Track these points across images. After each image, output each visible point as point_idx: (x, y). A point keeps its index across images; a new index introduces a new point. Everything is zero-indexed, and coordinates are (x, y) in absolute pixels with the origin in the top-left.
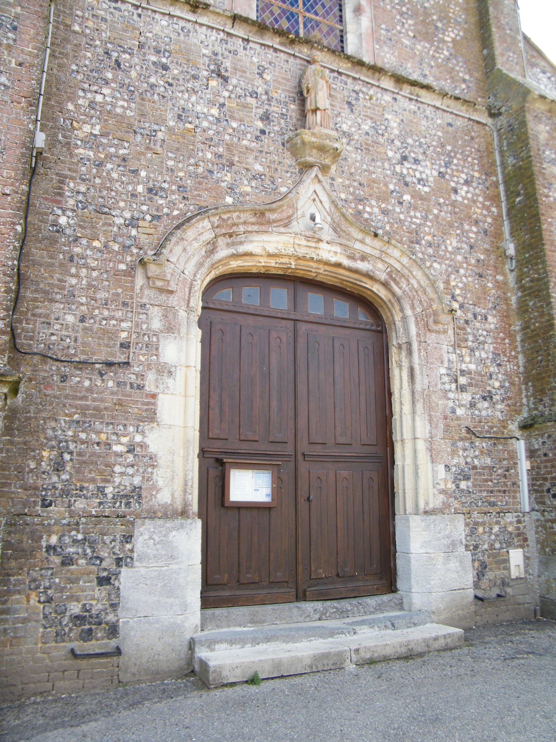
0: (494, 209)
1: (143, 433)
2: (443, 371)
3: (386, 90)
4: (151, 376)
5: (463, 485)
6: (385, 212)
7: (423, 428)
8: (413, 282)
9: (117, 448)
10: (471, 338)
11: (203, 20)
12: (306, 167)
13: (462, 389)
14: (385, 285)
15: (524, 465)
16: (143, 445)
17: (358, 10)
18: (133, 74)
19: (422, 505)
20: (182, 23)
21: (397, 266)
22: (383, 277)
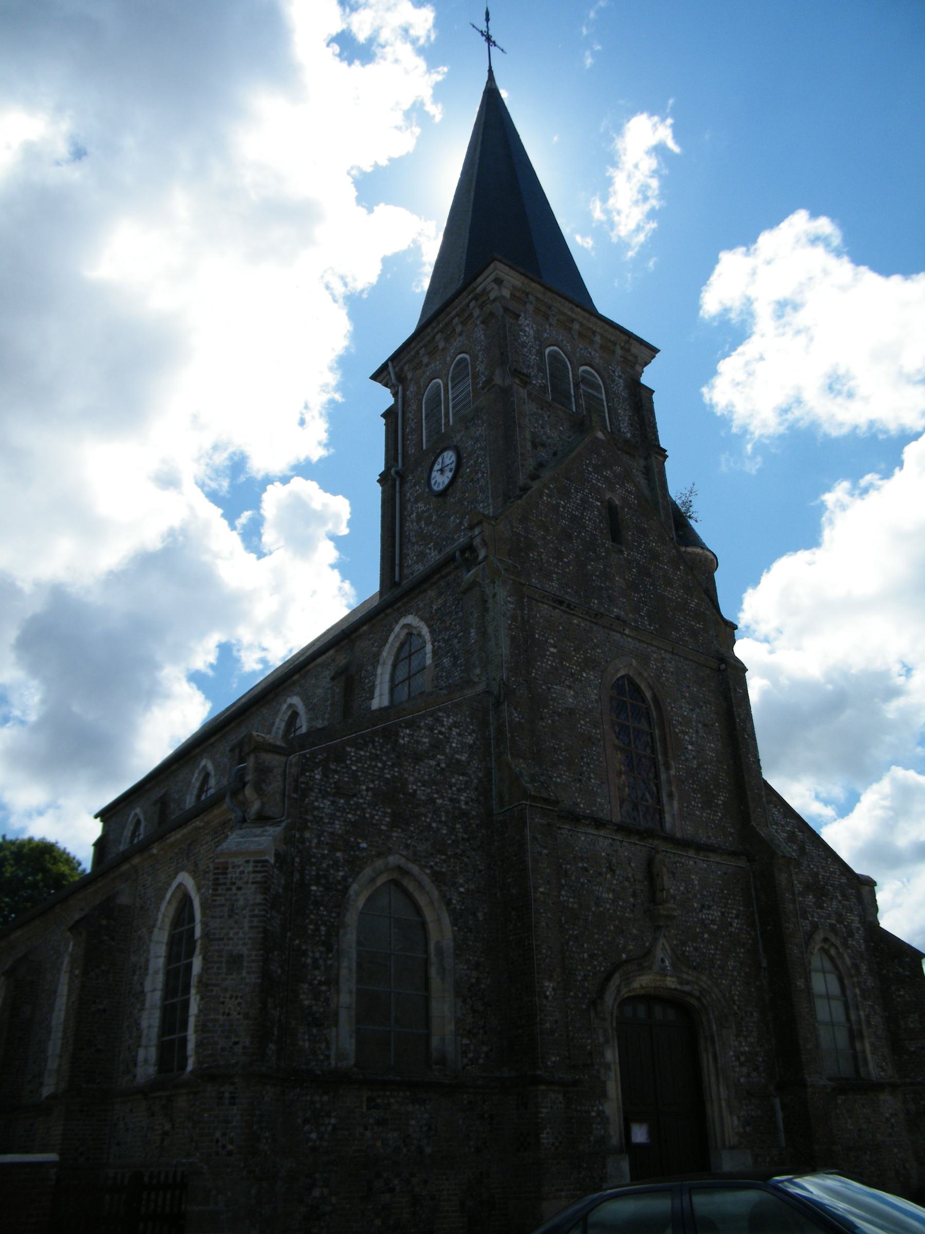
0: (753, 933)
1: (602, 1104)
2: (731, 1053)
3: (690, 857)
4: (602, 1071)
5: (748, 1129)
6: (696, 949)
7: (723, 1092)
8: (713, 995)
9: (593, 1114)
10: (744, 1029)
11: (602, 833)
12: (658, 928)
13: (742, 1065)
14: (698, 999)
15: (780, 1115)
16: (603, 1112)
17: (671, 795)
18: (573, 878)
19: (727, 1143)
20: (591, 837)
21: (705, 986)
22: (697, 994)
